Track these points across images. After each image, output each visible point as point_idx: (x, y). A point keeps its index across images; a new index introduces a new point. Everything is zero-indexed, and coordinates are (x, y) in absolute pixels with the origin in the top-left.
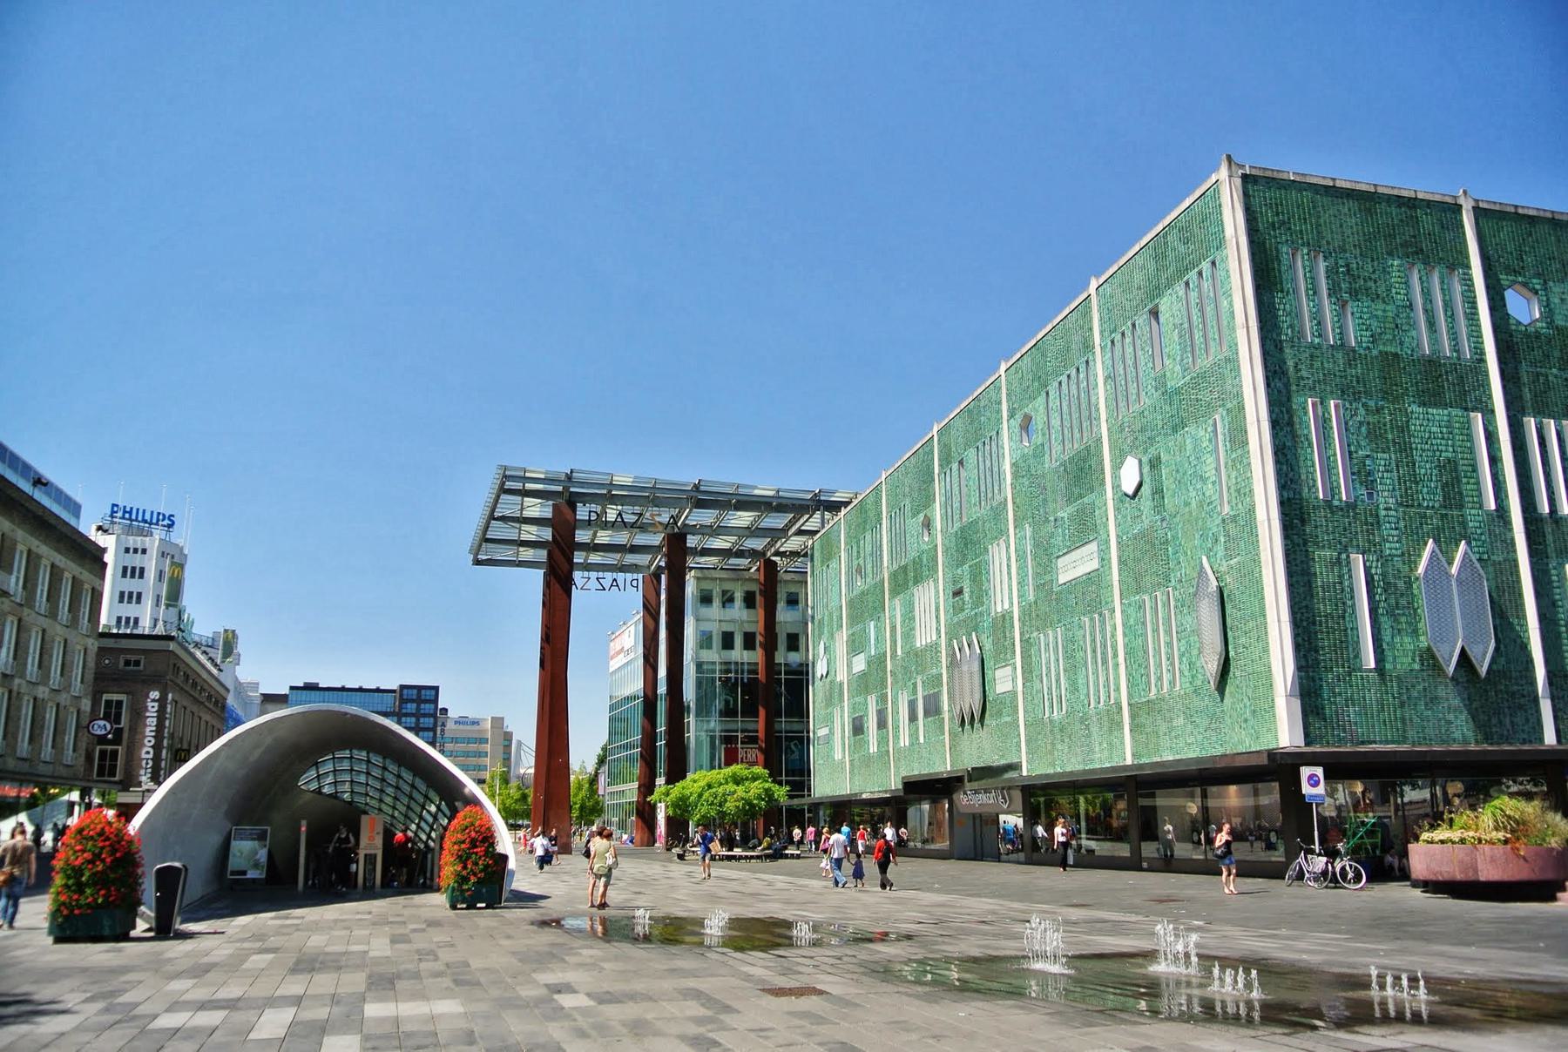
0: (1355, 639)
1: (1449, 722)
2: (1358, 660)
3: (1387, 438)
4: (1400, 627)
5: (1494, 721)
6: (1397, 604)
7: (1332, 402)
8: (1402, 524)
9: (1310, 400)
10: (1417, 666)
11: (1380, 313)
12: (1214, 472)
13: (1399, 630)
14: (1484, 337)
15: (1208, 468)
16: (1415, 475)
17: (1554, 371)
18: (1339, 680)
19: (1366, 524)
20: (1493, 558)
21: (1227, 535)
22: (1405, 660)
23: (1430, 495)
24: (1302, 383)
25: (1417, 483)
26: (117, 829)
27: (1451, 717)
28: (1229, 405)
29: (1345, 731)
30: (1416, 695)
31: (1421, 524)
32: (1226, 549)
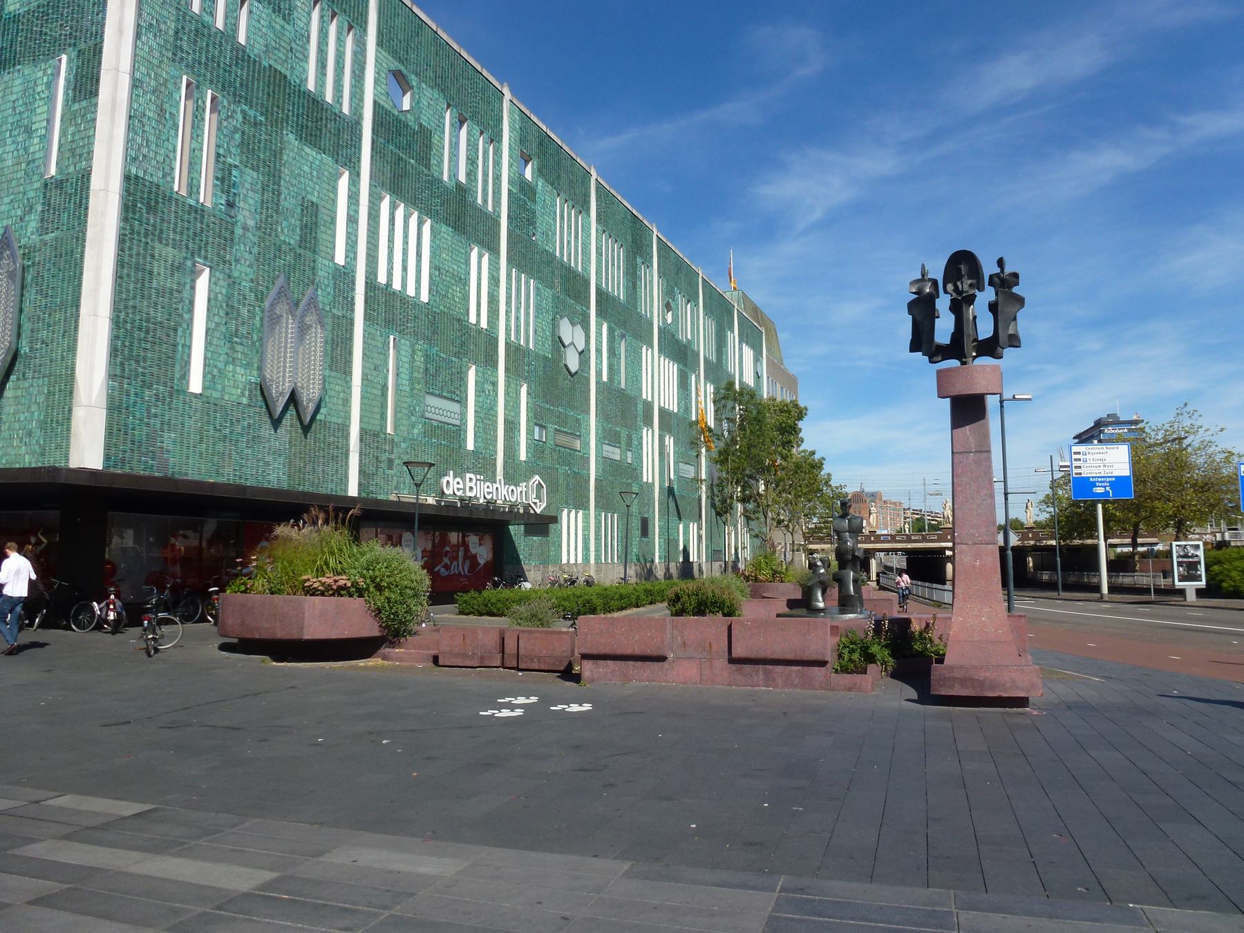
0: (186, 358)
1: (268, 464)
2: (184, 382)
3: (259, 157)
4: (235, 356)
5: (309, 468)
6: (237, 330)
7: (209, 92)
8: (255, 250)
9: (185, 77)
10: (245, 401)
11: (278, 27)
12: (45, 123)
13: (234, 359)
14: (365, 247)
15: (38, 118)
16: (278, 205)
17: (412, 161)
18: (158, 400)
19: (220, 237)
20: (335, 311)
21: (47, 203)
22: (234, 391)
23: (288, 233)
24: (179, 54)
25: (277, 212)
26: (599, 668)
27: (269, 458)
28: (82, 46)
29: (153, 458)
30: (239, 430)
31: (275, 256)
32: (42, 220)
